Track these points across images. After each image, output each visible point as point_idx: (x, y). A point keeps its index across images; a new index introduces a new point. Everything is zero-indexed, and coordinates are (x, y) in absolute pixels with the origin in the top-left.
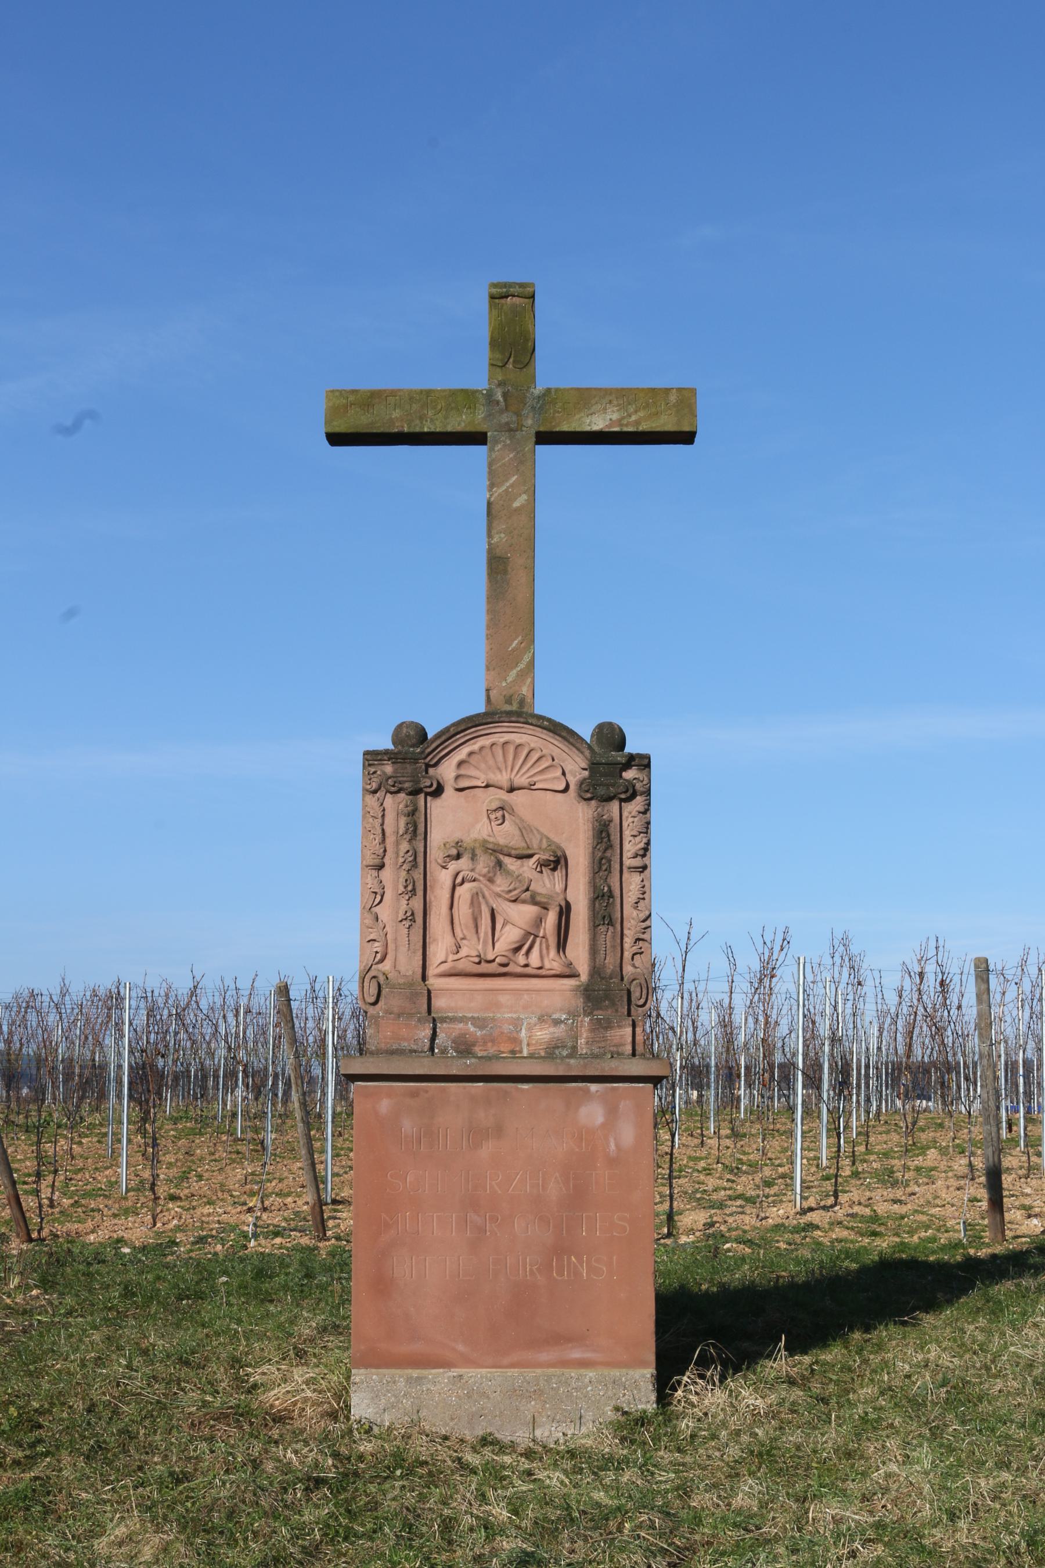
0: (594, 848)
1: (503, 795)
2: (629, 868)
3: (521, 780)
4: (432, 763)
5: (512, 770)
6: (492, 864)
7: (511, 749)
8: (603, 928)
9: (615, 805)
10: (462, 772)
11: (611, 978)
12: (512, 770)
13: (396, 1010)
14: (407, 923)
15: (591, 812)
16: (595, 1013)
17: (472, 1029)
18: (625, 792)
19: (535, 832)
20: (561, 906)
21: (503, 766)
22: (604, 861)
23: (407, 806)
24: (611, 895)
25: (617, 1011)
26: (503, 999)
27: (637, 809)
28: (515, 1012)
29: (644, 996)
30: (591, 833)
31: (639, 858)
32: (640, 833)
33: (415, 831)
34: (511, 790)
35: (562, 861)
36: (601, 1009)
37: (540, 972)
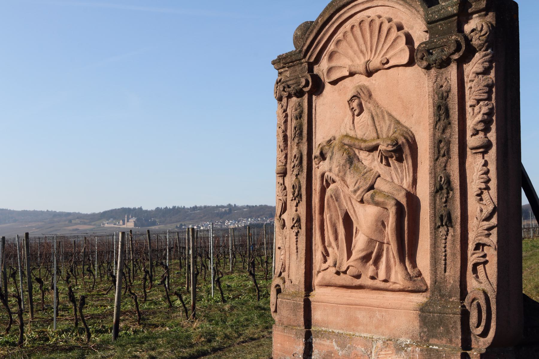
0: (435, 128)
1: (361, 80)
2: (472, 149)
3: (375, 63)
4: (312, 60)
5: (371, 51)
6: (342, 162)
7: (366, 25)
8: (442, 231)
9: (453, 69)
10: (333, 64)
11: (450, 297)
12: (371, 51)
13: (285, 323)
14: (295, 230)
15: (431, 85)
16: (432, 341)
17: (336, 348)
18: (458, 49)
19: (386, 117)
20: (398, 204)
21: (364, 49)
22: (442, 145)
23: (296, 110)
24: (185, 248)
25: (451, 341)
26: (361, 315)
27: (474, 69)
28: (370, 332)
29: (483, 323)
30: (432, 110)
31: (481, 135)
32: (478, 101)
33: (301, 134)
34: (369, 73)
35: (407, 150)
36: (436, 337)
37: (387, 285)
